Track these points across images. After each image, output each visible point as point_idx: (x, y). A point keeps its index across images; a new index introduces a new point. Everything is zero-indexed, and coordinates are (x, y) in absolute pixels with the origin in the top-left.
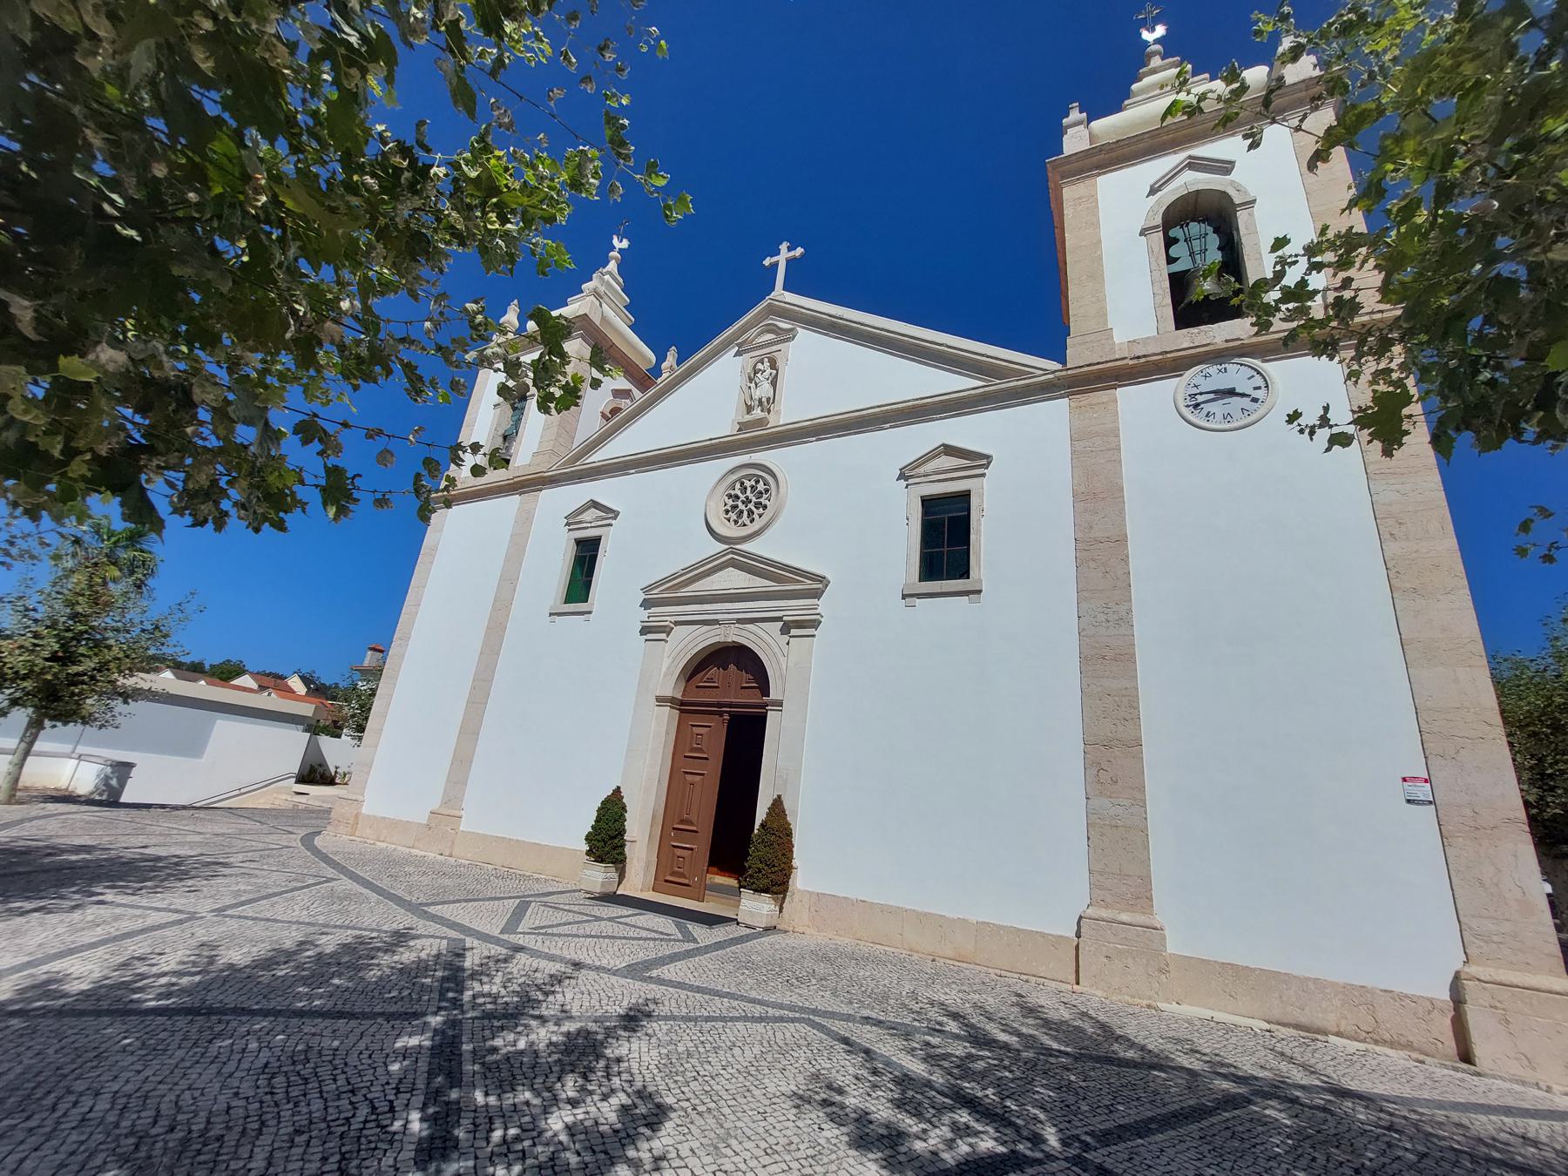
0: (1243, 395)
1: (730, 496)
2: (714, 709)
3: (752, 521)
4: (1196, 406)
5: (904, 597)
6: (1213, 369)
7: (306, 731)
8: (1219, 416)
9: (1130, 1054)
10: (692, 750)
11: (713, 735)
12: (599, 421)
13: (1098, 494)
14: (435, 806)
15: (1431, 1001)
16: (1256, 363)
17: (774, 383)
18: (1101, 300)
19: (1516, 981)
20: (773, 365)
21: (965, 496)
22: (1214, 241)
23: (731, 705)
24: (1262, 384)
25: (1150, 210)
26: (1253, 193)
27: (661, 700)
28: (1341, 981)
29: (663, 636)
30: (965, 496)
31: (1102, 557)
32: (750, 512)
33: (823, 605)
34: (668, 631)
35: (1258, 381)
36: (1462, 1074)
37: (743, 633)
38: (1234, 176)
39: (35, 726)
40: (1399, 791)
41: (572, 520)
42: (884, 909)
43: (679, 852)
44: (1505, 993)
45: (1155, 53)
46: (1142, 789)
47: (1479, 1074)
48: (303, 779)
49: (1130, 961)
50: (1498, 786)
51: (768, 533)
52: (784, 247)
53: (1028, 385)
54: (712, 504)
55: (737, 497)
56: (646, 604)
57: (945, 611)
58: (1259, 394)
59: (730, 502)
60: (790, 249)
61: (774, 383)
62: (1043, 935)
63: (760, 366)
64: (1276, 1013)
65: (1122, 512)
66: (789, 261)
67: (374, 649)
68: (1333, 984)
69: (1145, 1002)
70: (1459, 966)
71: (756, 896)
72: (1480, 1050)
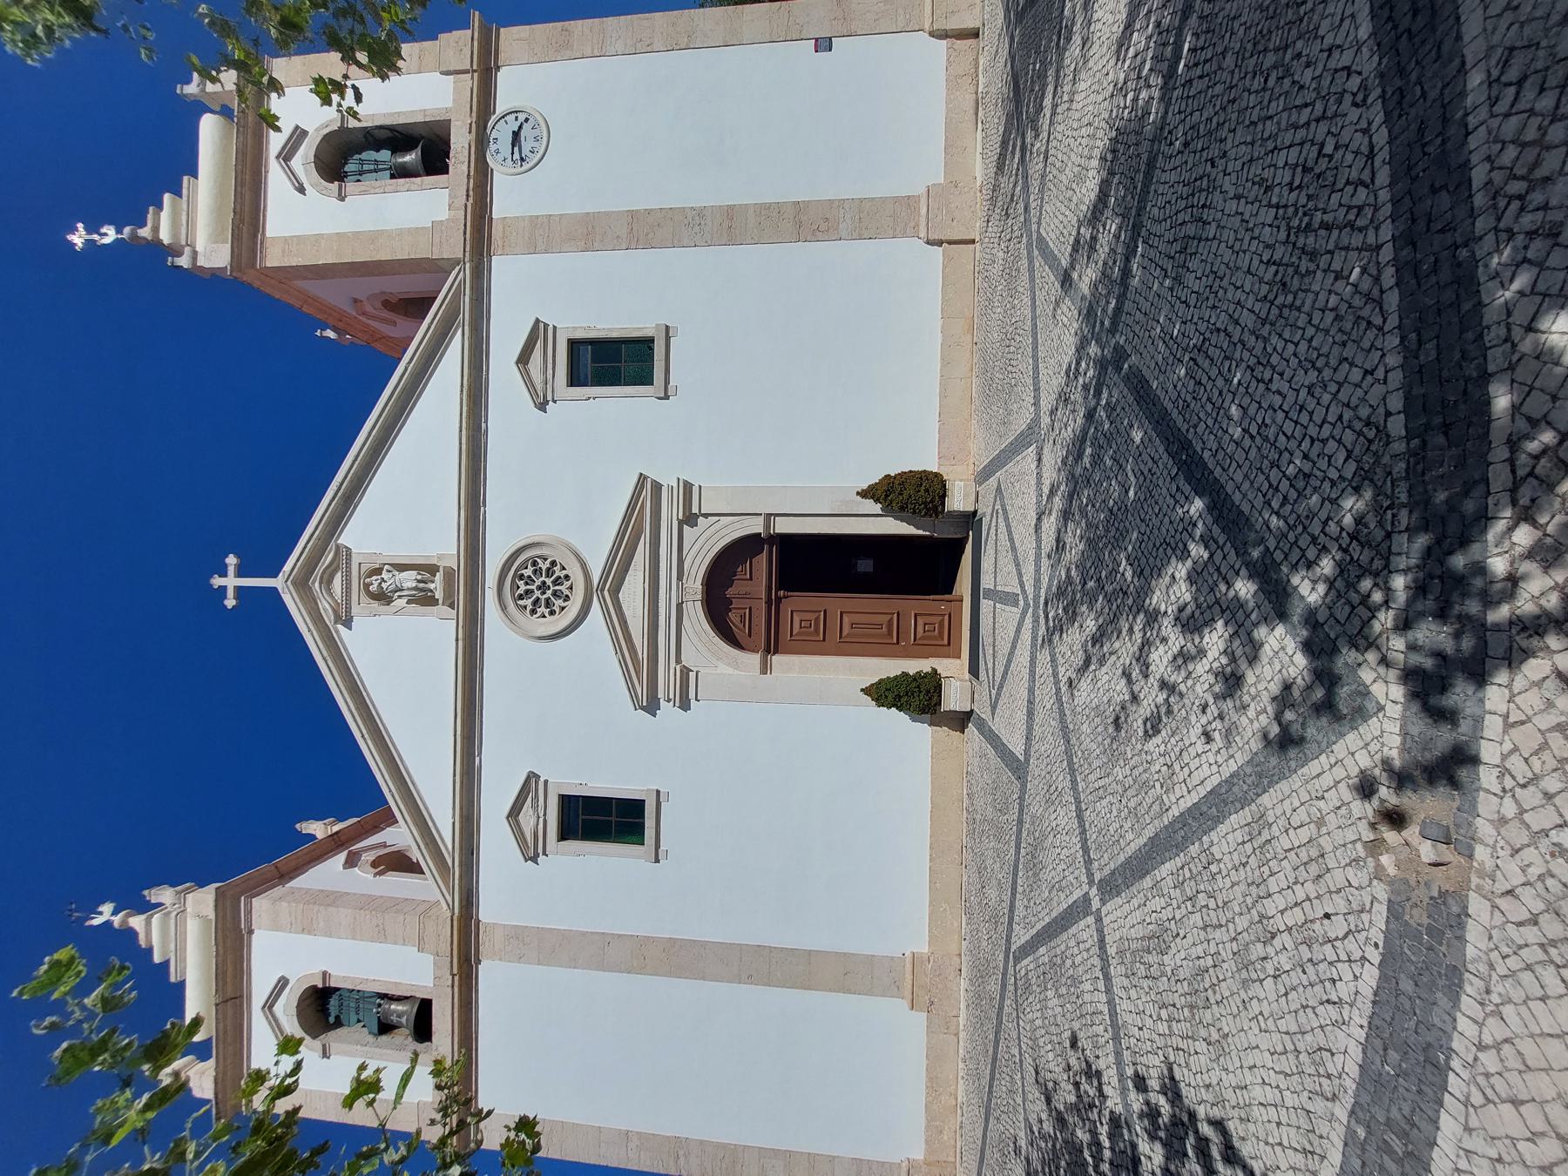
1: (533, 612)
2: (773, 604)
5: (657, 861)
6: (493, 147)
10: (817, 631)
11: (801, 607)
13: (590, 233)
14: (905, 1004)
16: (493, 118)
17: (402, 568)
18: (400, 232)
20: (378, 571)
21: (574, 344)
27: (765, 668)
29: (692, 675)
30: (574, 344)
31: (644, 230)
32: (557, 582)
33: (668, 480)
34: (686, 672)
35: (511, 118)
37: (693, 572)
39: (975, 512)
42: (943, 395)
44: (937, 12)
45: (124, 922)
51: (585, 555)
52: (217, 582)
53: (472, 288)
56: (652, 707)
57: (683, 362)
58: (522, 117)
59: (542, 610)
60: (224, 574)
61: (402, 568)
62: (944, 267)
64: (971, 125)
66: (240, 573)
71: (949, 493)
72: (970, 23)
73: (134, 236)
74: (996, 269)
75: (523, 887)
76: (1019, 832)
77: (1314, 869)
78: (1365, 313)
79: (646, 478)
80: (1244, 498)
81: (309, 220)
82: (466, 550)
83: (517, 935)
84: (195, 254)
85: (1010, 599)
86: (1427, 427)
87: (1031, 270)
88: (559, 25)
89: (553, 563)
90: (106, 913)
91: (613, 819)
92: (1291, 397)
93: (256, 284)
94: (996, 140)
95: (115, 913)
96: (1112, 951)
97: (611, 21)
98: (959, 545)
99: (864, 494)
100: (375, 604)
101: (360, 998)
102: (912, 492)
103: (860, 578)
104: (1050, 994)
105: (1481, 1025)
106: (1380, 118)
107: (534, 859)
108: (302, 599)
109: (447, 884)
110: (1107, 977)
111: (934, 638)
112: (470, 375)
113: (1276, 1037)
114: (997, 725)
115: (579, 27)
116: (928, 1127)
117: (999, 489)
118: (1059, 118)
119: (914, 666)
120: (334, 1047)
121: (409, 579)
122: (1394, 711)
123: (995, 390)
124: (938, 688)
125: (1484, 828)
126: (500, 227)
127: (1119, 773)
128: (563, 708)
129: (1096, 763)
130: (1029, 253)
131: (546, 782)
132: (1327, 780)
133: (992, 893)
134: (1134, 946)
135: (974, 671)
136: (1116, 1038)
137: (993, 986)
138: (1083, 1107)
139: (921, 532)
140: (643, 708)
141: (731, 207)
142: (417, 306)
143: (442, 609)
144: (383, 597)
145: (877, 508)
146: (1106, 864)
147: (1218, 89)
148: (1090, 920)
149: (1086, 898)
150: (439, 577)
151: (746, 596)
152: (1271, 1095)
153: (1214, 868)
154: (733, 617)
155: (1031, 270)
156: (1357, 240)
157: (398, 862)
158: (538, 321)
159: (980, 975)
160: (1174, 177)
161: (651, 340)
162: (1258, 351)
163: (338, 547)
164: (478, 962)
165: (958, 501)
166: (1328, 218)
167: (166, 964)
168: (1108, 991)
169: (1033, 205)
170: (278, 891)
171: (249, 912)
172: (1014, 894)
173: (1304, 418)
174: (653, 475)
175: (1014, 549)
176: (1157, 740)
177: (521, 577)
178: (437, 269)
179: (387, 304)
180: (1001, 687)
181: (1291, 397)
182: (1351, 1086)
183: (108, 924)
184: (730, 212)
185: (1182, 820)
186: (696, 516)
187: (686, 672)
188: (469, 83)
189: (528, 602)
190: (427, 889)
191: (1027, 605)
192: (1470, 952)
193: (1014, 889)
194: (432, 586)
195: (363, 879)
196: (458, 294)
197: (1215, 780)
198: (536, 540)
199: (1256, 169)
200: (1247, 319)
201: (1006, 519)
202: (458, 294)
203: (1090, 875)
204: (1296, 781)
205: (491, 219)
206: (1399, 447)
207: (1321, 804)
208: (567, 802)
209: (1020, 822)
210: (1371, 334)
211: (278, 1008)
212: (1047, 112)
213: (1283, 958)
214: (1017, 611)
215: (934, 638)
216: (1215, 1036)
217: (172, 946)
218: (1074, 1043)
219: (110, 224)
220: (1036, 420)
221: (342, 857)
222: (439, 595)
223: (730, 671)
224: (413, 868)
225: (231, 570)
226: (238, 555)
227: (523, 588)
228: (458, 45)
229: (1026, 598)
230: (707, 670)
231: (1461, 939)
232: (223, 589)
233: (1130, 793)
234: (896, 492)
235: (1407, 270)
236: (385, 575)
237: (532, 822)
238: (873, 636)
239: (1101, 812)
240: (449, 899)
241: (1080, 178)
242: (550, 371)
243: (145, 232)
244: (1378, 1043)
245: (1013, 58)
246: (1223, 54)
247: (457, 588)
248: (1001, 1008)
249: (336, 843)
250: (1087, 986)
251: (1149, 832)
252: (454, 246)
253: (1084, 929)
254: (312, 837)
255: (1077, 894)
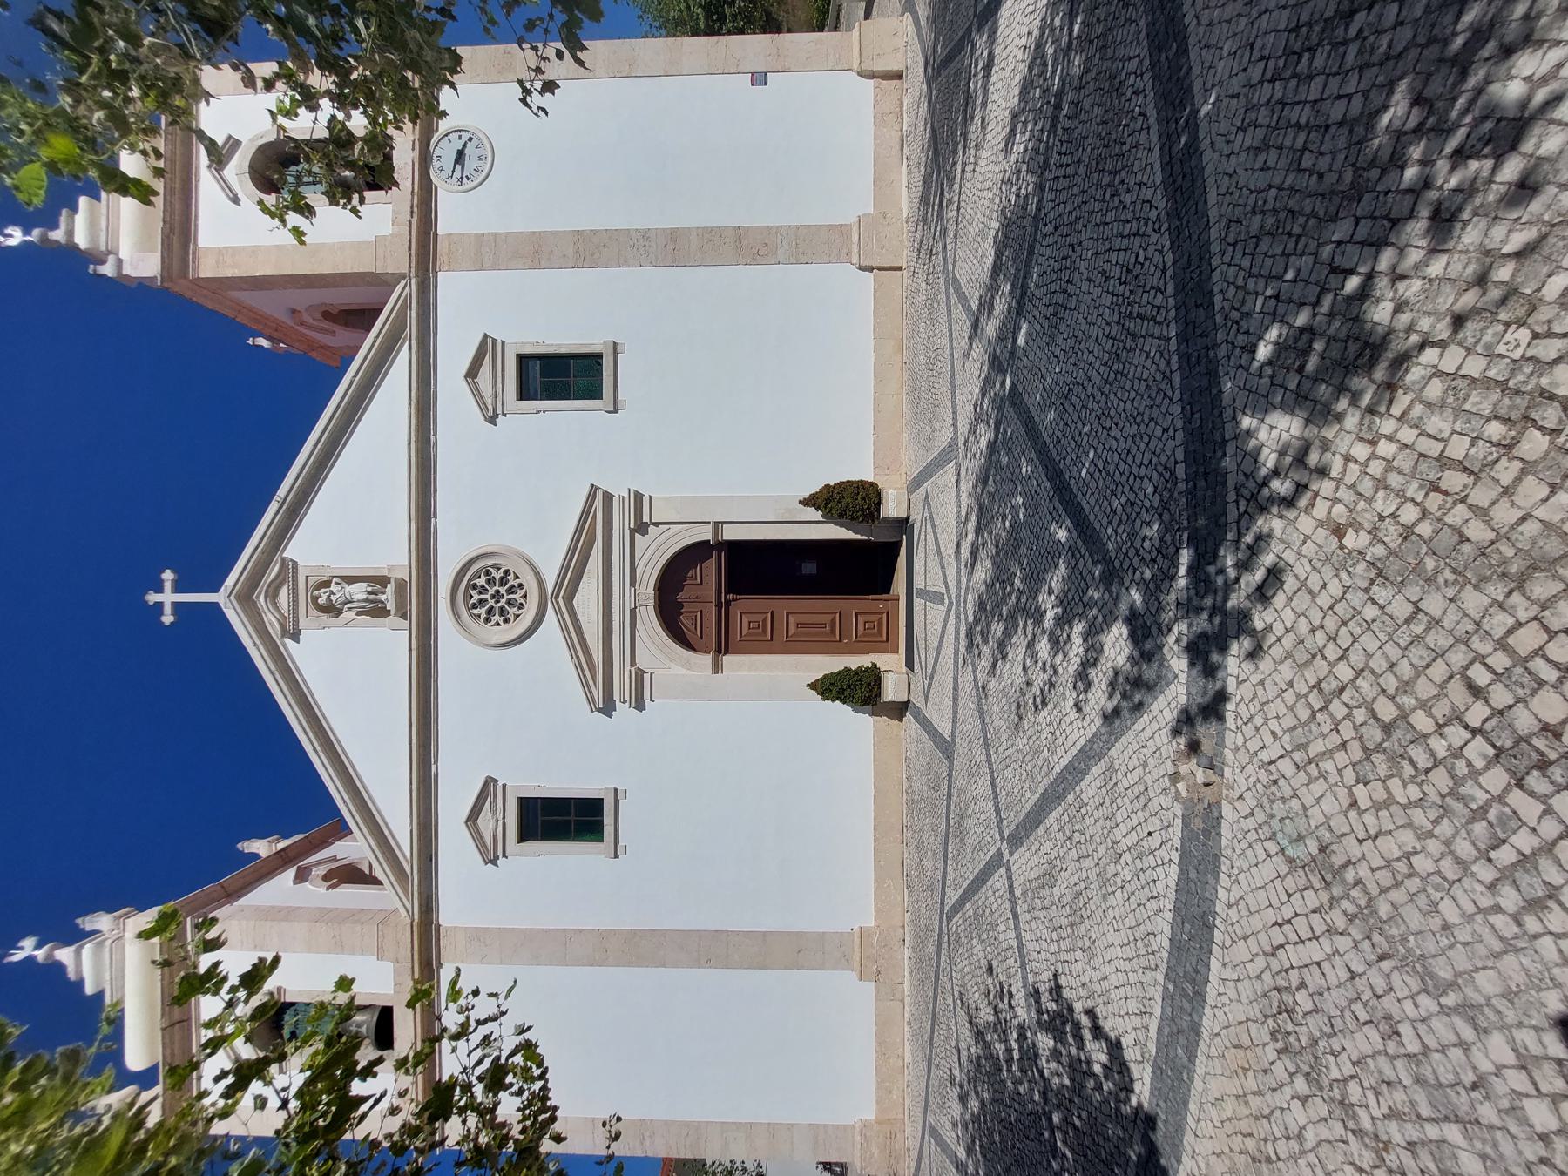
0: (464, 146)
2: (723, 607)
5: (616, 856)
6: (436, 164)
11: (750, 609)
13: (535, 251)
14: (854, 975)
16: (436, 137)
17: (351, 580)
20: (327, 584)
21: (522, 360)
27: (716, 668)
29: (647, 677)
30: (522, 360)
31: (588, 249)
32: (511, 590)
33: (619, 491)
35: (454, 136)
36: (909, 76)
42: (877, 411)
45: (50, 955)
50: (753, 46)
52: (152, 598)
56: (608, 709)
57: (630, 376)
58: (465, 136)
59: (496, 618)
60: (160, 590)
61: (351, 580)
66: (178, 588)
72: (895, 66)
73: (44, 239)
74: (921, 298)
75: (480, 890)
76: (949, 805)
77: (1142, 800)
78: (1163, 386)
79: (597, 488)
80: (1096, 519)
81: (237, 231)
82: (417, 561)
83: (478, 936)
84: (120, 262)
85: (937, 598)
86: (1196, 473)
87: (948, 305)
88: (501, 47)
89: (507, 572)
90: (27, 948)
91: (573, 818)
92: (1122, 444)
93: (188, 294)
94: (919, 178)
95: (38, 946)
96: (1018, 893)
98: (895, 547)
99: (806, 502)
100: (324, 617)
102: (850, 500)
103: (800, 583)
104: (975, 942)
105: (1229, 891)
106: (1168, 245)
107: (494, 862)
108: (245, 612)
109: (405, 891)
110: (1016, 917)
113: (1123, 933)
114: (930, 712)
116: (878, 1089)
117: (927, 497)
118: (968, 176)
119: (855, 662)
121: (358, 591)
122: (1183, 677)
123: (922, 407)
124: (878, 681)
125: (1228, 755)
127: (1020, 742)
128: (518, 712)
129: (1005, 736)
130: (947, 289)
131: (504, 786)
132: (1148, 733)
133: (928, 864)
134: (1034, 885)
135: (910, 664)
136: (1023, 966)
137: (931, 948)
138: (1000, 1026)
139: (859, 537)
140: (599, 710)
142: (362, 318)
143: (393, 619)
144: (331, 610)
145: (818, 515)
146: (1013, 819)
147: (1076, 190)
148: (1002, 870)
149: (999, 853)
150: (390, 588)
151: (698, 600)
152: (1121, 977)
153: (1083, 811)
155: (948, 305)
156: (1157, 331)
157: (351, 875)
158: (486, 336)
159: (920, 943)
160: (1048, 252)
161: (600, 356)
162: (1102, 404)
163: (283, 560)
164: (440, 965)
165: (892, 508)
166: (1142, 310)
167: (100, 995)
168: (1016, 927)
169: (949, 247)
172: (945, 862)
173: (1130, 461)
174: (604, 485)
175: (939, 553)
176: (1044, 713)
177: (474, 587)
178: (383, 283)
179: (327, 315)
180: (932, 678)
181: (1122, 444)
182: (1165, 955)
185: (1062, 776)
186: (647, 525)
187: (640, 674)
189: (482, 611)
190: (389, 899)
191: (951, 603)
192: (1224, 842)
193: (946, 857)
194: (383, 597)
195: (315, 892)
196: (405, 308)
197: (1082, 741)
198: (489, 550)
199: (1099, 261)
200: (1096, 378)
201: (933, 526)
202: (405, 308)
203: (1001, 833)
204: (1130, 735)
205: (436, 235)
206: (1182, 486)
207: (1145, 750)
208: (526, 805)
209: (949, 796)
210: (1166, 402)
212: (959, 168)
213: (1126, 872)
214: (943, 609)
216: (1087, 944)
217: (107, 976)
218: (990, 969)
219: (15, 224)
220: (955, 439)
221: (291, 873)
222: (391, 606)
223: (683, 671)
224: (371, 880)
225: (168, 586)
226: (174, 571)
227: (476, 597)
229: (950, 597)
230: (661, 672)
231: (1219, 834)
232: (160, 605)
233: (1028, 758)
234: (833, 501)
235: (1184, 357)
236: (333, 587)
237: (491, 825)
238: (816, 634)
239: (1009, 778)
240: (409, 906)
241: (984, 235)
243: (58, 235)
244: (1179, 919)
245: (932, 116)
246: (1079, 162)
247: (409, 599)
248: (938, 966)
249: (282, 861)
250: (1002, 928)
251: (1040, 790)
252: (398, 261)
253: (998, 880)
254: (255, 856)
255: (993, 850)
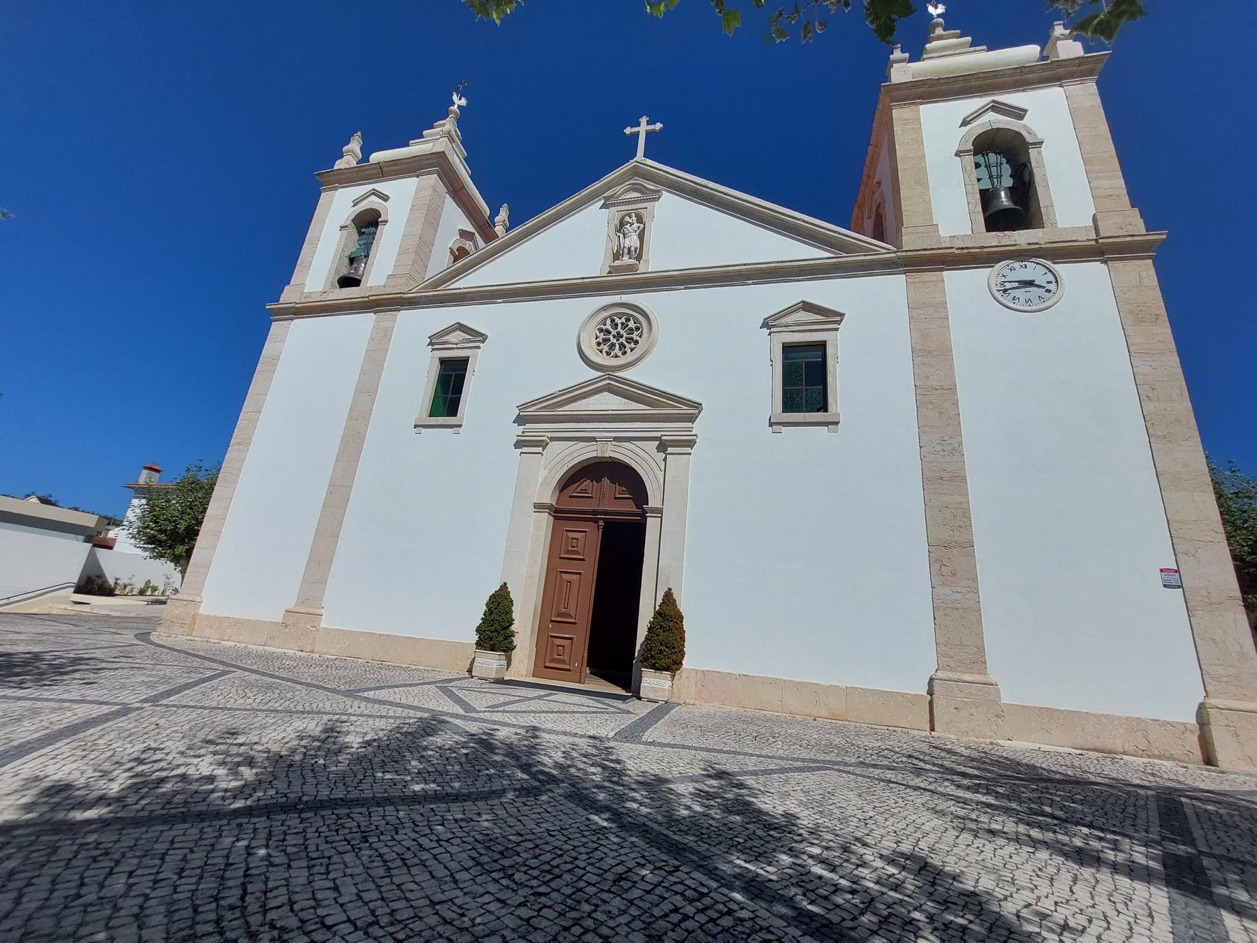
0: (1039, 286)
1: (601, 330)
2: (591, 517)
3: (625, 353)
4: (1005, 291)
6: (1017, 265)
7: (86, 541)
8: (1022, 300)
9: (1057, 776)
10: (568, 552)
11: (589, 540)
12: (447, 258)
14: (291, 605)
15: (1184, 725)
16: (1049, 263)
17: (641, 236)
19: (1241, 707)
20: (640, 219)
21: (822, 346)
22: (1007, 170)
23: (606, 513)
24: (1052, 279)
25: (960, 137)
26: (1040, 137)
27: (539, 507)
28: (1125, 715)
29: (540, 450)
30: (822, 346)
31: (937, 401)
32: (622, 346)
33: (697, 427)
34: (543, 445)
35: (1050, 277)
37: (619, 450)
38: (1026, 121)
40: (1158, 579)
41: (435, 341)
42: (765, 681)
43: (558, 642)
45: (938, 25)
46: (975, 579)
47: (1223, 772)
48: (79, 590)
49: (974, 710)
50: (1218, 571)
51: (641, 365)
52: (644, 120)
53: (862, 261)
54: (584, 336)
55: (608, 332)
56: (520, 420)
57: (806, 438)
58: (1052, 287)
59: (602, 336)
60: (649, 123)
61: (641, 236)
62: (903, 695)
63: (627, 219)
64: (1080, 742)
65: (951, 367)
66: (648, 133)
67: (146, 468)
68: (1119, 718)
69: (988, 741)
70: (1201, 700)
71: (658, 673)
72: (1223, 754)
75: (414, 339)
90: (459, 101)
93: (880, 107)
95: (459, 107)
97: (1175, 360)
100: (617, 222)
101: (367, 247)
102: (668, 649)
111: (552, 654)
112: (793, 267)
115: (1164, 331)
116: (216, 617)
120: (345, 232)
126: (935, 279)
139: (638, 647)
141: (964, 479)
150: (633, 261)
154: (587, 483)
161: (826, 410)
165: (652, 682)
170: (442, 188)
171: (429, 173)
183: (453, 104)
184: (958, 479)
188: (1086, 237)
189: (608, 327)
198: (654, 328)
211: (373, 198)
215: (552, 654)
222: (617, 263)
223: (540, 480)
228: (1128, 222)
232: (639, 125)
236: (636, 225)
237: (454, 340)
242: (796, 328)
252: (912, 241)
